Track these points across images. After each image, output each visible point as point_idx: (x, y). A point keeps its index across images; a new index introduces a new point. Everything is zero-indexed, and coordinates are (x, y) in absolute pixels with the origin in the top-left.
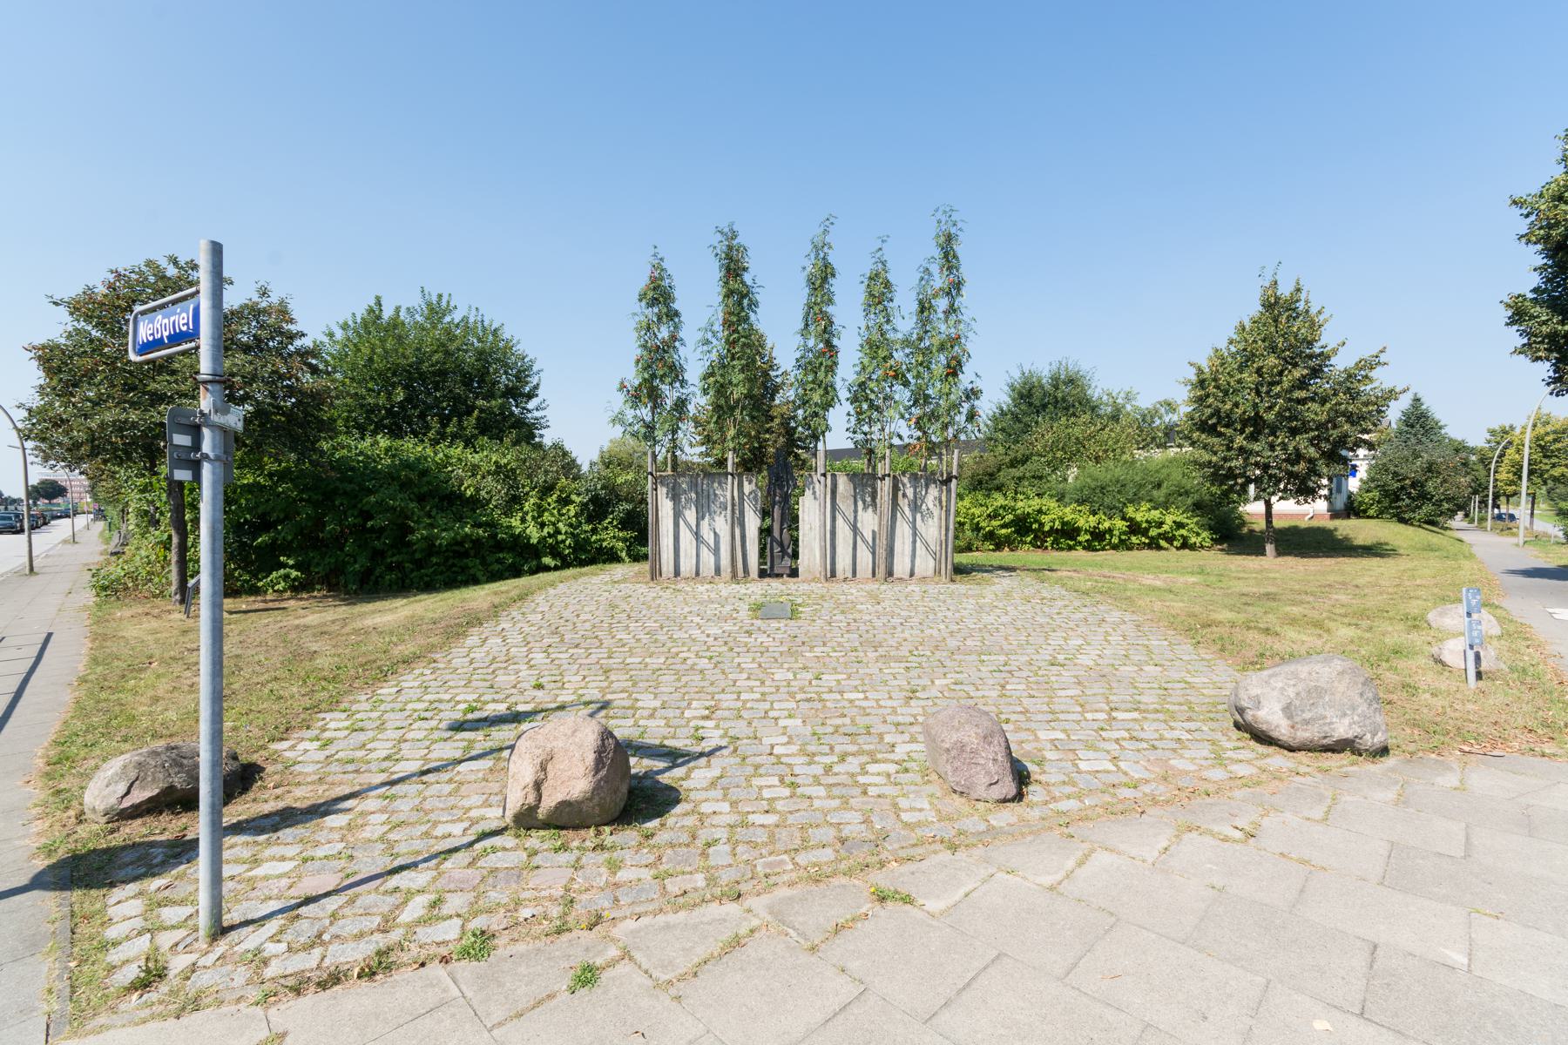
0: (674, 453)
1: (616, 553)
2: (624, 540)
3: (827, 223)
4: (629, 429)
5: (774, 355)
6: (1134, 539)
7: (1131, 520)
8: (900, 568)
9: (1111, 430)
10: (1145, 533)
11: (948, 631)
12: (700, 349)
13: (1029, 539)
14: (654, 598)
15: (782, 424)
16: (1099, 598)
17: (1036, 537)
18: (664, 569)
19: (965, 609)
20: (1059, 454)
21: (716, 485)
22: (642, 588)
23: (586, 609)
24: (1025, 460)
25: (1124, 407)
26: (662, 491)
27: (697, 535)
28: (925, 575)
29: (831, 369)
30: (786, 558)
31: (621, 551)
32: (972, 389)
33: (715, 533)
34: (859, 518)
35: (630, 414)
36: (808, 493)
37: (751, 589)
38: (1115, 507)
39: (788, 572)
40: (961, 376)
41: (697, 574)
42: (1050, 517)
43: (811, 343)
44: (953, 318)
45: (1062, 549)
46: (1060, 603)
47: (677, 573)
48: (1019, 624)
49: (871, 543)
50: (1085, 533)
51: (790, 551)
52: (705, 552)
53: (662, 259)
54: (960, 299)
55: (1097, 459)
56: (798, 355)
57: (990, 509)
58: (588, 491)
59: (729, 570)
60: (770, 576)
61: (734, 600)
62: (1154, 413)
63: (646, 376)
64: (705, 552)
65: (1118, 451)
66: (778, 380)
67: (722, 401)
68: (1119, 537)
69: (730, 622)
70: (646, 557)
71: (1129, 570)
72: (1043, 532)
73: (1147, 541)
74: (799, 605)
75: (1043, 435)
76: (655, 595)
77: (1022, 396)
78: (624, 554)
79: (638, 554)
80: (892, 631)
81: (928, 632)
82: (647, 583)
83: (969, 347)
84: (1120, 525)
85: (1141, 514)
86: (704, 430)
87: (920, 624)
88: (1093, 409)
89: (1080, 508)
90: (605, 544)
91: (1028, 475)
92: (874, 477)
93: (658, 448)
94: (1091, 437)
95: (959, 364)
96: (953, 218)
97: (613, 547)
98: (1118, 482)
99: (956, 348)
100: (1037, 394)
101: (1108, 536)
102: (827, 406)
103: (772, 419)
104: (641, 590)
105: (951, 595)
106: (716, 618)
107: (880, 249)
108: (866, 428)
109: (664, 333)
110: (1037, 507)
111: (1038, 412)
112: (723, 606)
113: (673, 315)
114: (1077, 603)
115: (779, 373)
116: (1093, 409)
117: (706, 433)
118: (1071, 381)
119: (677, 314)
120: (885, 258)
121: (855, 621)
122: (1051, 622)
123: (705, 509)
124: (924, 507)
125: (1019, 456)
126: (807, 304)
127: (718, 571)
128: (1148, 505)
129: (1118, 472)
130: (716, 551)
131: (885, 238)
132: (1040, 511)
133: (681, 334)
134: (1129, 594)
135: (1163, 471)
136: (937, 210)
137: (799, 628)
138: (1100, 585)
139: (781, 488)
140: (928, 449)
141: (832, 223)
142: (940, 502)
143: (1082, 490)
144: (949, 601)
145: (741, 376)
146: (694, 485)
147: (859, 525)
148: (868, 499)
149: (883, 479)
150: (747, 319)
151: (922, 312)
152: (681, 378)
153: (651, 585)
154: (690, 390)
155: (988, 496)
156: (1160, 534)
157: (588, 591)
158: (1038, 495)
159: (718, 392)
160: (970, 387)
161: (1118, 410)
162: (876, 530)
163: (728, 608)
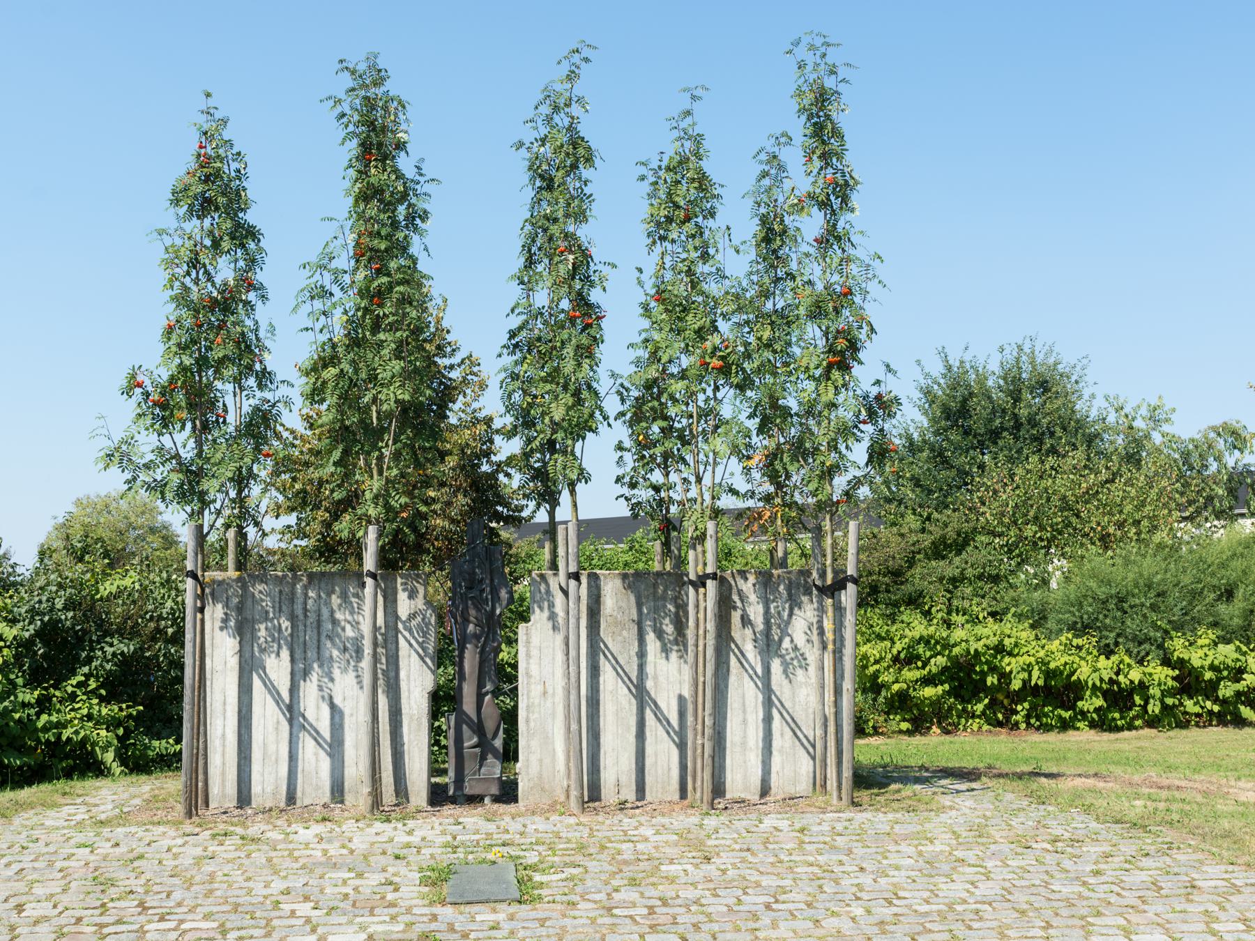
0: (240, 528)
1: (93, 752)
2: (112, 724)
3: (576, 58)
4: (144, 477)
5: (445, 324)
6: (1190, 705)
7: (1181, 663)
8: (739, 777)
9: (1129, 482)
10: (1210, 690)
11: (872, 920)
12: (307, 308)
13: (979, 708)
14: (198, 861)
15: (463, 468)
16: (1170, 835)
17: (993, 704)
18: (214, 790)
19: (897, 868)
20: (1030, 530)
21: (335, 600)
22: (167, 837)
23: (39, 890)
24: (962, 543)
25: (1147, 436)
26: (215, 612)
27: (292, 712)
28: (792, 791)
29: (586, 352)
30: (490, 759)
31: (105, 749)
32: (879, 397)
33: (333, 706)
34: (649, 669)
35: (147, 443)
36: (539, 617)
37: (419, 834)
38: (1148, 639)
39: (495, 790)
40: (856, 370)
41: (291, 799)
42: (1021, 660)
43: (541, 298)
44: (836, 254)
45: (1047, 728)
46: (1093, 850)
47: (244, 798)
48: (1021, 898)
49: (675, 722)
50: (1093, 694)
51: (498, 743)
52: (309, 749)
53: (225, 122)
54: (849, 216)
55: (1105, 541)
56: (515, 321)
57: (898, 646)
58: (33, 612)
59: (366, 789)
60: (454, 801)
61: (383, 860)
62: (1205, 449)
63: (188, 361)
64: (309, 749)
65: (1145, 523)
66: (454, 374)
67: (353, 419)
68: (1162, 702)
69: (383, 914)
70: (169, 762)
71: (1199, 772)
72: (1009, 695)
73: (1216, 708)
74: (534, 868)
75: (995, 492)
76: (198, 851)
77: (947, 413)
78: (109, 757)
79: (144, 755)
80: (751, 925)
81: (830, 923)
82: (176, 824)
83: (871, 311)
84: (1162, 675)
85: (1201, 653)
86: (294, 479)
87: (809, 905)
88: (1091, 440)
89: (1079, 641)
90: (66, 733)
91: (970, 572)
92: (678, 579)
93: (208, 518)
94: (1090, 495)
95: (854, 346)
96: (829, 60)
97: (85, 740)
98: (1149, 586)
99: (846, 312)
100: (979, 408)
101: (1138, 700)
102: (581, 428)
103: (443, 455)
104: (166, 842)
105: (860, 835)
106: (347, 905)
107: (688, 113)
108: (657, 477)
109: (225, 271)
110: (993, 641)
111: (981, 443)
112: (360, 875)
113: (244, 235)
114: (1128, 848)
115: (456, 360)
116: (1091, 440)
117: (298, 486)
118: (1044, 385)
119: (252, 233)
120: (698, 130)
121: (665, 903)
122: (1086, 893)
123: (311, 654)
124: (786, 644)
125: (951, 533)
126: (531, 221)
127: (338, 791)
128: (1212, 635)
129: (1150, 565)
130: (335, 748)
131: (698, 92)
132: (999, 649)
133: (260, 276)
134: (1226, 824)
135: (1234, 564)
136: (797, 43)
137: (542, 922)
138: (1162, 806)
139: (479, 603)
140: (787, 521)
141: (587, 60)
142: (821, 632)
143: (1081, 604)
144: (859, 851)
145: (397, 365)
146: (286, 601)
147: (649, 684)
148: (669, 629)
149: (701, 582)
150: (404, 248)
151: (767, 240)
152: (258, 367)
153: (188, 828)
154: (279, 394)
155: (892, 618)
156: (1238, 694)
157: (40, 847)
158: (993, 614)
159: (344, 397)
160: (874, 391)
161: (1138, 443)
162: (686, 693)
163: (374, 879)
